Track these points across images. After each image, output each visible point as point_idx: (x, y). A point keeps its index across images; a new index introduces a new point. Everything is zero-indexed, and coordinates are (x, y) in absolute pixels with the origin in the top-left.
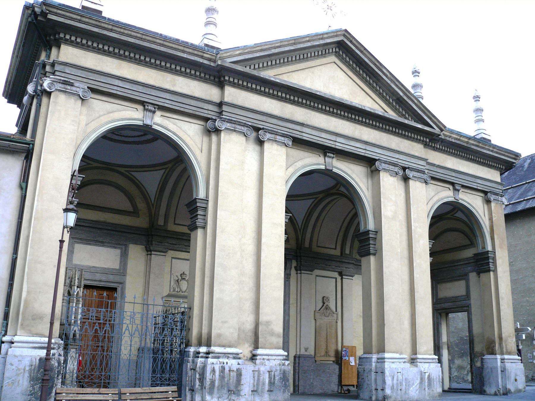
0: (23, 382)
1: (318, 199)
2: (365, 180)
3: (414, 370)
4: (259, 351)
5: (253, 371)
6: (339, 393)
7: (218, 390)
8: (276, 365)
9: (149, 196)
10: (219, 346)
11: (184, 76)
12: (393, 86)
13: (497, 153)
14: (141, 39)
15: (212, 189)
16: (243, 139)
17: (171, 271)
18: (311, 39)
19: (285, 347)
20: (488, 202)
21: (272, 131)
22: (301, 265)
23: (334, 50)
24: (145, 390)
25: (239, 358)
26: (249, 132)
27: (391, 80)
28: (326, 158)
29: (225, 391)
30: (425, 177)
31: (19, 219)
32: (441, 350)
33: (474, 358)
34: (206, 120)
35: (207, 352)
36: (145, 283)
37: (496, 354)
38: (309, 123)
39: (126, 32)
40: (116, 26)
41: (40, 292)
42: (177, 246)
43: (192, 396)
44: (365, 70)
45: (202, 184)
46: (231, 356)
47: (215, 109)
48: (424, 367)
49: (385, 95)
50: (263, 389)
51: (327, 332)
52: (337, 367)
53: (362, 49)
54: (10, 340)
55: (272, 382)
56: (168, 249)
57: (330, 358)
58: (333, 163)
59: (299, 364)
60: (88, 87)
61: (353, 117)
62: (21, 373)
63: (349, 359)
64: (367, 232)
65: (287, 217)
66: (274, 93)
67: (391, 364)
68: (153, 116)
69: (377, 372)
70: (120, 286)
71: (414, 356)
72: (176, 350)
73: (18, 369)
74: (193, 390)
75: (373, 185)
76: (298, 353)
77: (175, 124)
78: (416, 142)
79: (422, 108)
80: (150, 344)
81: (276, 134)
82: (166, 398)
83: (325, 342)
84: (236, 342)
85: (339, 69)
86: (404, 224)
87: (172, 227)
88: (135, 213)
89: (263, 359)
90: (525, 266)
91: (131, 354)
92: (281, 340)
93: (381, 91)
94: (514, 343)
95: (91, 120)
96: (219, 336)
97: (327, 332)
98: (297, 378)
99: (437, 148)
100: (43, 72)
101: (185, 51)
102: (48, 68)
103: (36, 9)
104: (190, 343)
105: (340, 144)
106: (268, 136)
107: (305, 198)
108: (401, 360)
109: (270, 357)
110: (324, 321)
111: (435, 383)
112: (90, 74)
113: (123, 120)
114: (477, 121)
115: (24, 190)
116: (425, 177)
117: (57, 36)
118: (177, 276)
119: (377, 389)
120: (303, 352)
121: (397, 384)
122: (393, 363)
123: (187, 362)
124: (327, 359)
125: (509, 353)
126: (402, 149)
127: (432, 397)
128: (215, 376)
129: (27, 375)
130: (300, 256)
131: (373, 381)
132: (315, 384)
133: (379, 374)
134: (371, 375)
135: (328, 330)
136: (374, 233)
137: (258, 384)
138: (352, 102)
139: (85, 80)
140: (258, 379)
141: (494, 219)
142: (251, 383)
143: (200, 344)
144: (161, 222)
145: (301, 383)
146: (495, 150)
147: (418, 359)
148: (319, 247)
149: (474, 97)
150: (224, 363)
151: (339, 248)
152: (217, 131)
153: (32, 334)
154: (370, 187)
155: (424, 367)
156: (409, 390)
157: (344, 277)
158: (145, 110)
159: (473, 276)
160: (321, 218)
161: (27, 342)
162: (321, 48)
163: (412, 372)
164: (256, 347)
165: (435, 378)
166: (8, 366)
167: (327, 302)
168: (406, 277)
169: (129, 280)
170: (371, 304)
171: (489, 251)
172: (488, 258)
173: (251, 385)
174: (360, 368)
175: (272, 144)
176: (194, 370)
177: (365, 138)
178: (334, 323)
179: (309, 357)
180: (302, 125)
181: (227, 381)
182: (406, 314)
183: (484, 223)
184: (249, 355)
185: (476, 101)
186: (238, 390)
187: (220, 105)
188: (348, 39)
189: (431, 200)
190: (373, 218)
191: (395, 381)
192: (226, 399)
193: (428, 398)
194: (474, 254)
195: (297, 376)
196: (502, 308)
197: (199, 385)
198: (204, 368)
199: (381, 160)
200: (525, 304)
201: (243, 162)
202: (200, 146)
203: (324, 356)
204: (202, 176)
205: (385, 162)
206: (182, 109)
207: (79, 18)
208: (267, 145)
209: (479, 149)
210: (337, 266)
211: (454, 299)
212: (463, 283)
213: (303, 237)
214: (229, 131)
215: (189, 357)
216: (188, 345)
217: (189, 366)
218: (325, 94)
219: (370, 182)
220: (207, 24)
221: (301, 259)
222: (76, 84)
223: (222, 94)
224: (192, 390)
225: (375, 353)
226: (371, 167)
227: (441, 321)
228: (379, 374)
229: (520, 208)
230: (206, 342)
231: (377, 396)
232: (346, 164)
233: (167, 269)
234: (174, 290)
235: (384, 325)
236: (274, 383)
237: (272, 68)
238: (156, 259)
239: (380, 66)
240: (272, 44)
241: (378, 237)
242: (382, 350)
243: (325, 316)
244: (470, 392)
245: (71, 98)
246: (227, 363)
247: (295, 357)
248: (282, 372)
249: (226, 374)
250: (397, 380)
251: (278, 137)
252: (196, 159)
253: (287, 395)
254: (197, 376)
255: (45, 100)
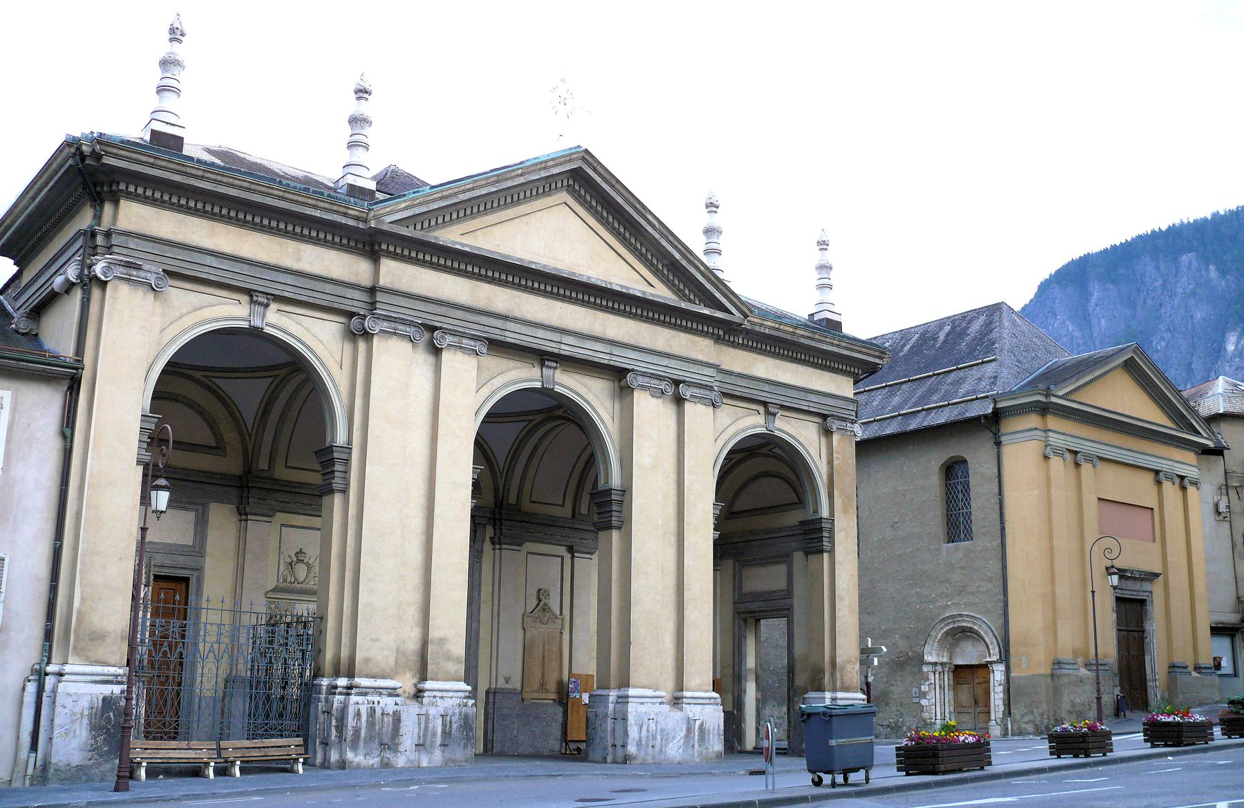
0: (80, 733)
1: (534, 423)
2: (608, 404)
3: (677, 715)
4: (428, 685)
5: (418, 715)
6: (563, 754)
7: (365, 743)
8: (453, 706)
9: (242, 417)
10: (368, 676)
11: (315, 244)
12: (664, 243)
13: (846, 348)
14: (248, 190)
15: (357, 430)
16: (407, 346)
17: (280, 548)
18: (526, 171)
19: (470, 676)
20: (828, 433)
21: (455, 331)
22: (501, 533)
23: (565, 183)
24: (256, 743)
25: (398, 695)
26: (418, 335)
27: (662, 234)
28: (544, 369)
29: (376, 745)
30: (712, 395)
31: (62, 485)
32: (743, 682)
33: (793, 696)
34: (351, 315)
35: (349, 685)
36: (237, 569)
37: (824, 691)
38: (518, 314)
39: (225, 180)
40: (209, 172)
41: (100, 598)
42: (292, 505)
43: (325, 753)
44: (617, 215)
45: (341, 421)
46: (384, 692)
47: (365, 297)
48: (692, 711)
49: (650, 258)
50: (433, 742)
51: (544, 650)
52: (559, 710)
53: (614, 182)
54: (57, 671)
55: (447, 731)
56: (275, 510)
57: (549, 694)
58: (556, 376)
59: (494, 705)
60: (164, 271)
61: (592, 300)
62: (78, 719)
63: (581, 697)
64: (608, 492)
65: (477, 470)
66: (461, 267)
67: (638, 705)
68: (266, 312)
69: (616, 719)
70: (195, 573)
71: (678, 694)
72: (295, 681)
73: (74, 714)
74: (327, 744)
75: (622, 410)
76: (493, 686)
77: (300, 324)
78: (700, 336)
79: (713, 279)
80: (243, 670)
81: (463, 335)
82: (288, 755)
83: (540, 668)
84: (392, 670)
85: (573, 213)
86: (673, 476)
87: (281, 473)
88: (218, 448)
89: (434, 697)
90: (917, 530)
91: (203, 687)
92: (462, 668)
93: (644, 250)
94: (857, 672)
95: (169, 323)
96: (367, 661)
97: (544, 650)
98: (490, 728)
99: (738, 344)
100: (90, 244)
101: (318, 207)
102: (100, 240)
103: (84, 148)
104: (321, 673)
105: (568, 347)
106: (449, 339)
107: (512, 419)
108: (655, 700)
109: (444, 694)
110: (539, 631)
111: (711, 736)
112: (167, 248)
113: (217, 320)
114: (821, 287)
115: (69, 440)
116: (712, 395)
117: (114, 188)
118: (290, 556)
119: (616, 746)
120: (501, 684)
121: (647, 737)
122: (642, 703)
123: (317, 701)
124: (543, 695)
125: (846, 689)
126: (675, 350)
127: (704, 759)
128: (361, 722)
129: (86, 721)
130: (500, 520)
131: (609, 732)
132: (521, 737)
133: (619, 721)
134: (606, 722)
135: (547, 646)
136: (619, 492)
137: (425, 735)
138: (589, 278)
139: (159, 259)
140: (426, 728)
141: (835, 463)
142: (415, 732)
143: (337, 674)
144: (263, 465)
145: (498, 736)
146: (843, 344)
147: (685, 698)
148: (535, 502)
149: (819, 243)
150: (373, 703)
151: (569, 504)
152: (367, 335)
153: (90, 662)
154: (617, 415)
155: (692, 711)
156: (666, 747)
157: (576, 555)
158: (252, 302)
159: (798, 557)
160: (539, 453)
161: (83, 674)
162: (543, 183)
163: (673, 719)
164: (424, 678)
165: (711, 728)
166: (58, 709)
167: (545, 598)
168: (671, 565)
169: (209, 564)
170: (610, 609)
171: (822, 518)
172: (821, 530)
173: (415, 736)
174: (591, 712)
175: (454, 353)
176: (328, 713)
177: (612, 333)
178: (557, 634)
179: (511, 692)
180: (506, 318)
181: (379, 729)
182: (670, 626)
183: (818, 470)
184: (412, 691)
185: (821, 249)
186: (396, 744)
187: (372, 290)
188: (589, 164)
189: (723, 434)
190: (619, 470)
191: (644, 733)
192: (378, 756)
193: (698, 760)
194: (800, 522)
195: (490, 724)
196: (838, 614)
197: (336, 736)
198: (344, 709)
199: (636, 371)
200: (913, 600)
201: (407, 385)
202: (338, 358)
203: (538, 691)
204: (341, 408)
205: (644, 374)
206: (311, 300)
207: (152, 160)
208: (446, 356)
209: (813, 344)
210: (565, 537)
211: (768, 596)
212: (782, 569)
213: (507, 487)
214: (386, 335)
215: (320, 693)
216: (317, 674)
217: (320, 708)
218: (545, 266)
219: (617, 406)
220: (352, 145)
221: (501, 524)
222: (146, 267)
223: (375, 270)
224: (325, 744)
225: (615, 688)
226: (620, 380)
227: (745, 631)
228: (619, 721)
229: (913, 425)
230: (346, 672)
231: (615, 756)
232: (578, 377)
233: (274, 545)
234: (285, 580)
235: (630, 643)
236: (450, 733)
237: (459, 223)
238: (256, 528)
239: (643, 209)
240: (461, 186)
241: (626, 499)
242: (625, 683)
243: (542, 623)
244: (785, 754)
245: (138, 289)
246: (379, 703)
247: (487, 692)
248: (463, 716)
249: (377, 719)
250: (648, 731)
251: (465, 341)
252: (333, 381)
253: (470, 752)
254: (334, 722)
255: (96, 293)
